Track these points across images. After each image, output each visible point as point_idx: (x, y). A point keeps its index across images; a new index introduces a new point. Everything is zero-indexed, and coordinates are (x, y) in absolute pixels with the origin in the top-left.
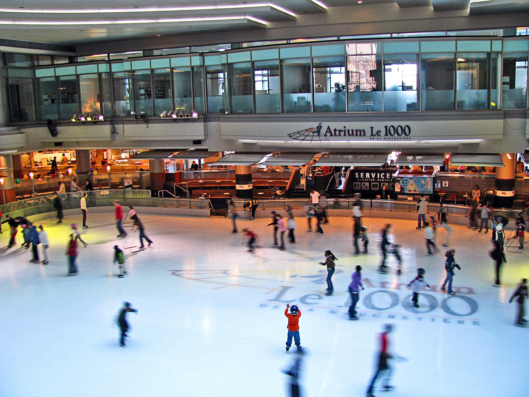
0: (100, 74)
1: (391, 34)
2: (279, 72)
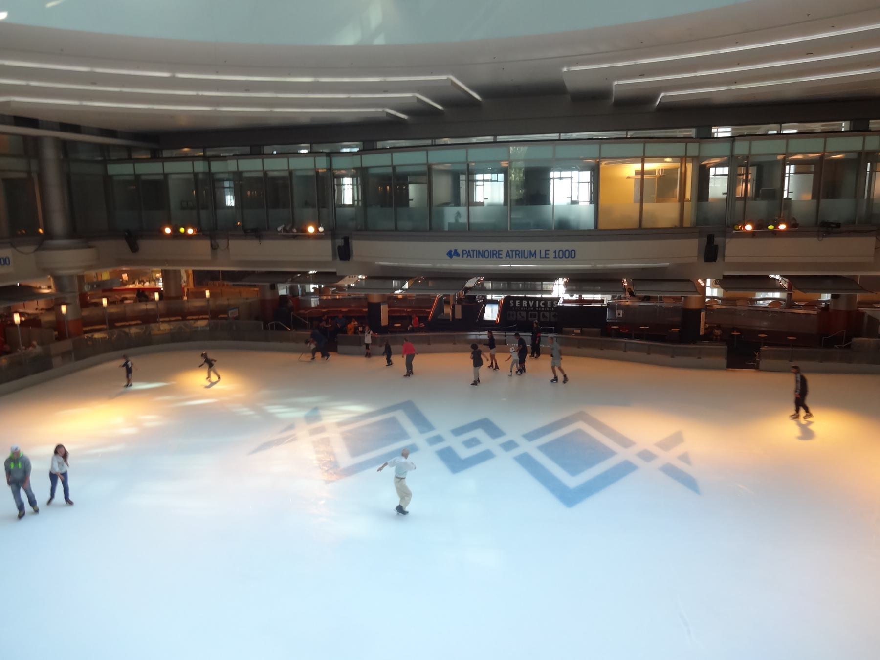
0: (196, 174)
1: (779, 134)
2: (425, 178)
